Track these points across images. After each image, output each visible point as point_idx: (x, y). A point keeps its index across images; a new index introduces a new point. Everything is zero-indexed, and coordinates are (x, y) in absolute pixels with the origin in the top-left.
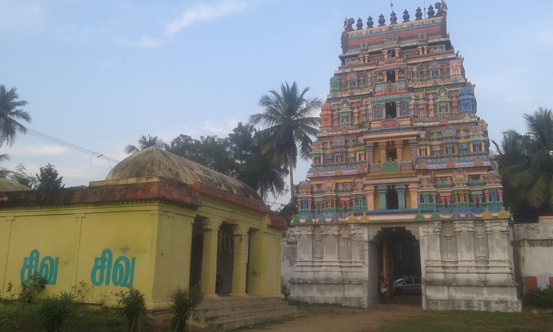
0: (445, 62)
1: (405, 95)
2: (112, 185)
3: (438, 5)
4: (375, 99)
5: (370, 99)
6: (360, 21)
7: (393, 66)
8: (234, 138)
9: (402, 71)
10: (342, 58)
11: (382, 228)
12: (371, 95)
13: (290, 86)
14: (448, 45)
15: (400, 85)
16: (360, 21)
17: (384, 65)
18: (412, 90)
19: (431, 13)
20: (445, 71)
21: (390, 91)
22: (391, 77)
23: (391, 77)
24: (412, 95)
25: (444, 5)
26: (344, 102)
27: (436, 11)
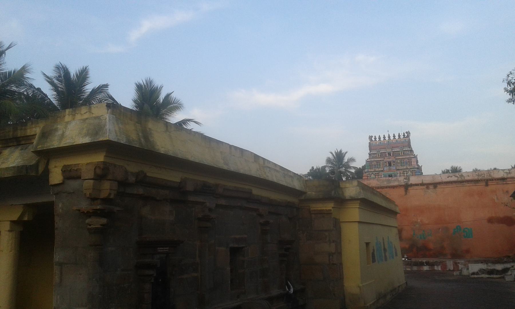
0: (409, 159)
1: (396, 172)
2: (19, 168)
3: (407, 133)
4: (385, 173)
5: (382, 173)
6: (375, 137)
7: (391, 160)
8: (309, 174)
9: (394, 162)
10: (370, 154)
11: (27, 206)
12: (382, 171)
13: (339, 151)
14: (412, 151)
15: (393, 168)
16: (375, 137)
17: (387, 159)
18: (398, 170)
19: (404, 135)
20: (410, 163)
21: (390, 170)
22: (390, 164)
23: (390, 164)
24: (398, 172)
25: (410, 133)
26: (372, 174)
27: (406, 135)
